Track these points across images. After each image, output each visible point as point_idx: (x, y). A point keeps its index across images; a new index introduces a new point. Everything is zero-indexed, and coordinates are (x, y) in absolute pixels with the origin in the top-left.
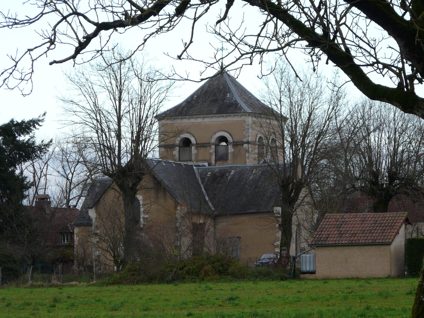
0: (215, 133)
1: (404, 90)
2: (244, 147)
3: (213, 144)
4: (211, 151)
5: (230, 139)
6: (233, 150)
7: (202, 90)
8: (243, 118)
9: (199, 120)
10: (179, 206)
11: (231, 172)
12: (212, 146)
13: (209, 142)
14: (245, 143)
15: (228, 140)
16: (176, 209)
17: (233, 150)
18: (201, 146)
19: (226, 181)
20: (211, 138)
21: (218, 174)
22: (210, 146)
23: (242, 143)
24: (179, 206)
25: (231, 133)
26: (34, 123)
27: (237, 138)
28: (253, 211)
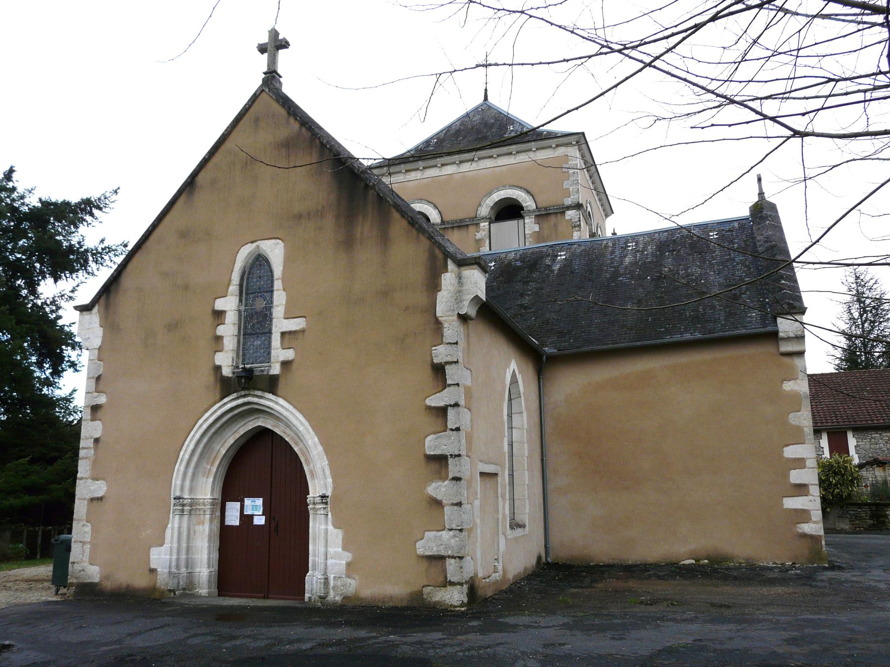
0: (490, 194)
1: (267, 511)
2: (567, 218)
3: (483, 219)
4: (479, 236)
5: (528, 203)
6: (536, 228)
7: (448, 131)
8: (561, 151)
9: (449, 170)
10: (451, 265)
11: (557, 256)
12: (482, 224)
13: (473, 215)
14: (569, 208)
15: (524, 205)
16: (434, 286)
17: (536, 228)
18: (453, 228)
19: (548, 276)
20: (480, 205)
21: (519, 264)
22: (477, 224)
23: (562, 210)
24: (451, 265)
25: (529, 190)
26: (88, 206)
27: (547, 200)
28: (688, 336)
